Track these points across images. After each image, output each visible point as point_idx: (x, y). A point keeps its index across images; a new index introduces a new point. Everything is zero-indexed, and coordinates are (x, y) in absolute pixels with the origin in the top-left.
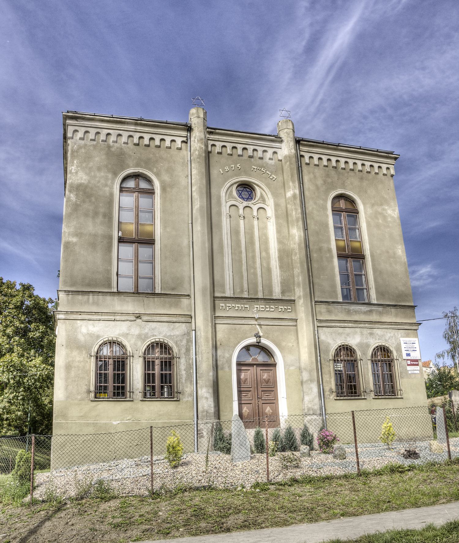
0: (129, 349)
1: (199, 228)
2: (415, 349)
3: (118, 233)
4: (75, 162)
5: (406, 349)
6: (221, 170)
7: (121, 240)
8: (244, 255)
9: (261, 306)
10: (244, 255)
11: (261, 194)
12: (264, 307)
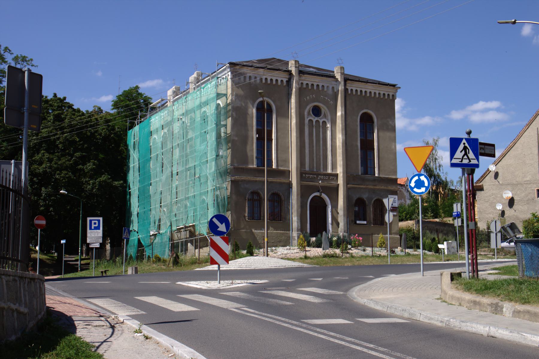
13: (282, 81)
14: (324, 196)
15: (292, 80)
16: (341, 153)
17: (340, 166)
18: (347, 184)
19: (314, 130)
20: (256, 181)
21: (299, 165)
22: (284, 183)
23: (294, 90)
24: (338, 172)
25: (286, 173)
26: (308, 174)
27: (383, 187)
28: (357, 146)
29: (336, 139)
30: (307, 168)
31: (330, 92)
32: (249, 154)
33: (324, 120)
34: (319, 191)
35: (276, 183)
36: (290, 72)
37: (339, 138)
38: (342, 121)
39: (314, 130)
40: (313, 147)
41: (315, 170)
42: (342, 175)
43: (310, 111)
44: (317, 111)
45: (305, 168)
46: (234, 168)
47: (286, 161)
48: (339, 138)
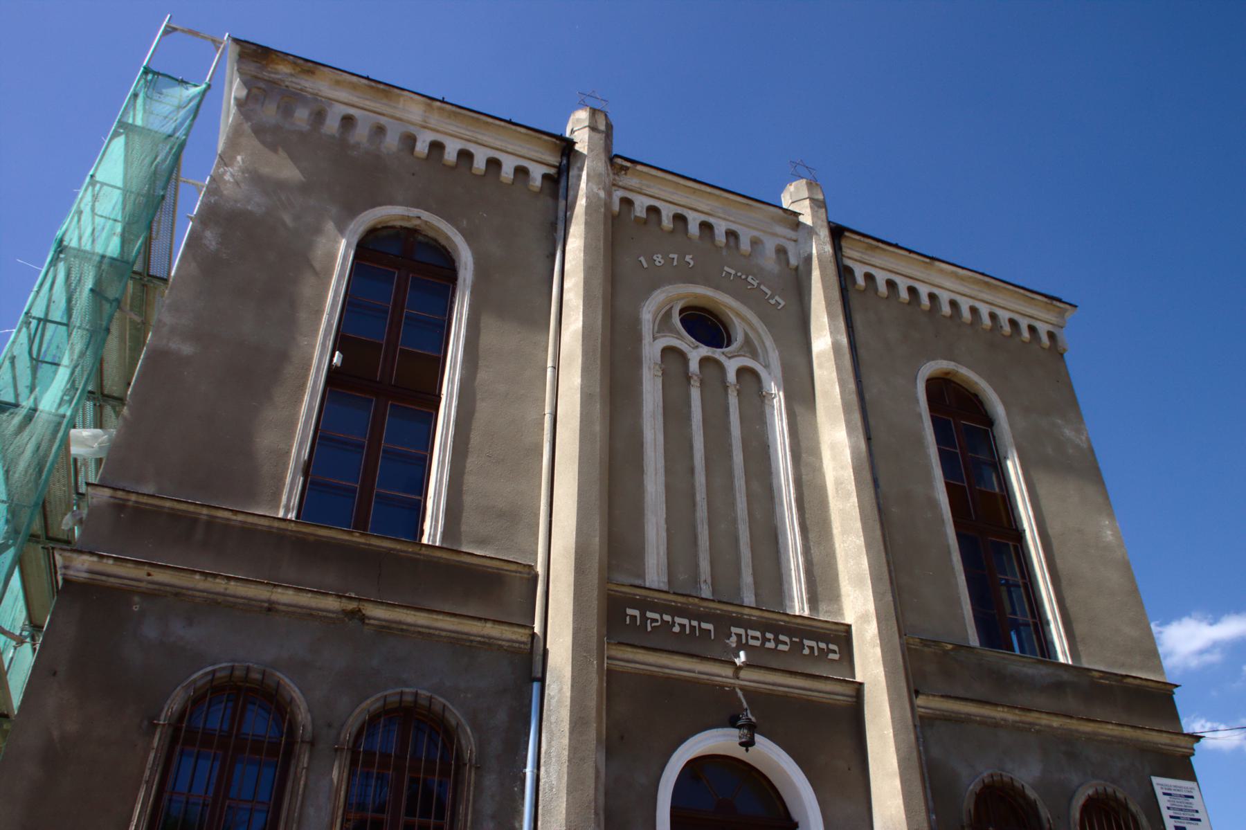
0: (303, 716)
1: (485, 138)
2: (1196, 816)
3: (332, 356)
4: (239, 158)
5: (1171, 813)
6: (642, 259)
7: (121, 400)
8: (700, 478)
9: (751, 633)
10: (700, 478)
11: (746, 335)
12: (758, 634)
13: (521, 172)
14: (770, 755)
15: (573, 173)
16: (856, 513)
17: (858, 582)
18: (915, 692)
19: (695, 394)
20: (270, 608)
21: (596, 542)
22: (488, 644)
23: (581, 203)
24: (849, 619)
25: (513, 588)
26: (655, 607)
27: (1110, 730)
28: (934, 504)
29: (816, 452)
30: (655, 573)
31: (769, 261)
32: (266, 440)
33: (748, 362)
34: (733, 722)
35: (427, 636)
36: (567, 147)
37: (833, 447)
38: (839, 369)
39: (695, 394)
40: (692, 470)
41: (706, 592)
42: (872, 629)
43: (668, 315)
44: (706, 325)
45: (641, 575)
46: (119, 507)
47: (519, 519)
48: (833, 447)
